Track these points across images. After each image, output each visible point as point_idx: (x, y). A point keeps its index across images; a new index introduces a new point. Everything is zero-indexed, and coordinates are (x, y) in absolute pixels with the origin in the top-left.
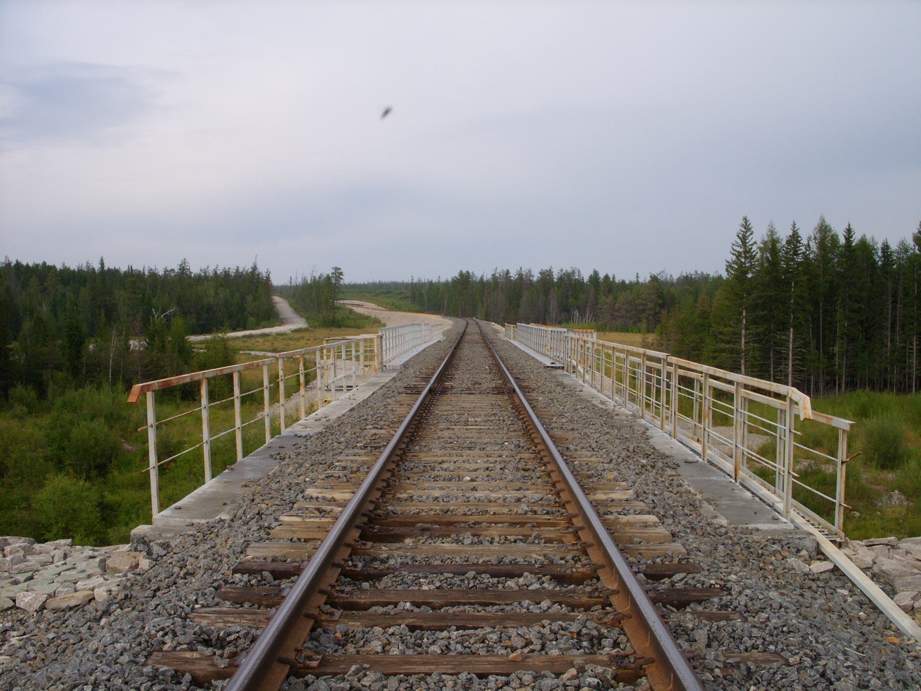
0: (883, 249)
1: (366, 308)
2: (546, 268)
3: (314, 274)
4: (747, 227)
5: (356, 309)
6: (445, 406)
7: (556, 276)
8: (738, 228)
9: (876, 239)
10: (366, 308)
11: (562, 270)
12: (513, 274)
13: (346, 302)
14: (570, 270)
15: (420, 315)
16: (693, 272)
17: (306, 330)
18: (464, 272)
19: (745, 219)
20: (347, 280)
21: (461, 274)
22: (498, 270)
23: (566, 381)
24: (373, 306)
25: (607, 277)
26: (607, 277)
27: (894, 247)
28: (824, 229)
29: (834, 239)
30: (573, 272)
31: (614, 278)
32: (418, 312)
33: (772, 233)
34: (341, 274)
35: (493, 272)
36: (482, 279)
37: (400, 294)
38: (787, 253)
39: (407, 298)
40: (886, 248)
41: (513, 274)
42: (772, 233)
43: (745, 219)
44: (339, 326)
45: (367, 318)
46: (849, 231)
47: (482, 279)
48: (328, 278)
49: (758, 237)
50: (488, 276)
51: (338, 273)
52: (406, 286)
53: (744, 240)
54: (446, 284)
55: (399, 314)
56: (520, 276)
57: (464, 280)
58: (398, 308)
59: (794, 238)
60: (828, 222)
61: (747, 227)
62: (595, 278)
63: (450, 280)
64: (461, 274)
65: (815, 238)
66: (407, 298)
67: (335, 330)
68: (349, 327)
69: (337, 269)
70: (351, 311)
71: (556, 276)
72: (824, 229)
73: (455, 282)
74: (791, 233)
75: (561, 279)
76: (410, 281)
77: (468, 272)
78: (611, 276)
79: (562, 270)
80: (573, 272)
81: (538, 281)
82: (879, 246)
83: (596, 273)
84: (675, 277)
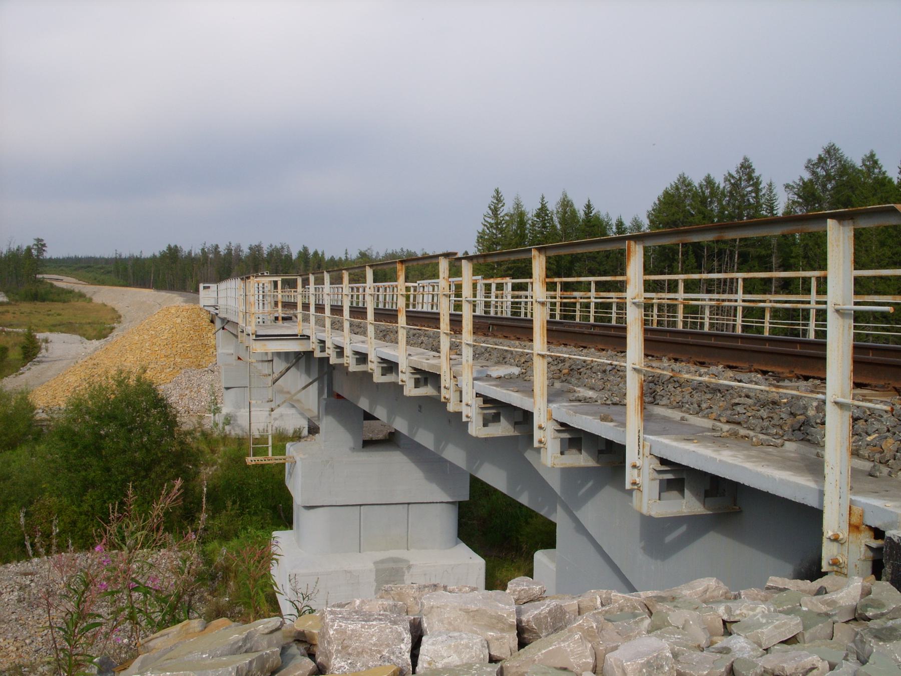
0: (617, 225)
1: (66, 282)
2: (255, 243)
3: (12, 246)
4: (498, 198)
5: (56, 283)
6: (252, 413)
7: (265, 251)
8: (490, 200)
9: (611, 215)
10: (66, 282)
11: (271, 246)
12: (222, 250)
13: (46, 276)
14: (279, 246)
15: (129, 289)
16: (399, 250)
17: (8, 304)
18: (172, 246)
19: (497, 192)
20: (51, 253)
21: (169, 248)
22: (208, 245)
23: (519, 369)
24: (74, 280)
25: (316, 253)
26: (316, 253)
27: (627, 223)
28: (566, 204)
29: (574, 213)
30: (282, 248)
31: (323, 254)
32: (127, 286)
33: (518, 206)
34: (44, 245)
35: (201, 247)
36: (190, 253)
37: (101, 268)
38: (534, 225)
39: (109, 272)
40: (620, 224)
41: (222, 250)
42: (518, 206)
43: (497, 192)
44: (43, 300)
45: (71, 292)
46: (589, 206)
47: (190, 253)
48: (29, 249)
49: (508, 208)
50: (196, 251)
51: (41, 245)
52: (107, 261)
53: (495, 211)
54: (154, 259)
55: (105, 289)
56: (229, 250)
57: (173, 253)
58: (103, 283)
59: (543, 211)
60: (570, 197)
61: (498, 198)
62: (304, 254)
63: (158, 254)
64: (169, 248)
65: (558, 212)
66: (109, 272)
67: (39, 305)
68: (53, 301)
69: (39, 240)
70: (52, 285)
71: (265, 251)
72: (566, 204)
73: (163, 256)
74: (540, 206)
75: (270, 254)
76: (114, 256)
77: (176, 246)
78: (320, 253)
79: (271, 246)
80: (282, 248)
81: (247, 257)
82: (614, 222)
83: (305, 249)
84: (382, 254)
